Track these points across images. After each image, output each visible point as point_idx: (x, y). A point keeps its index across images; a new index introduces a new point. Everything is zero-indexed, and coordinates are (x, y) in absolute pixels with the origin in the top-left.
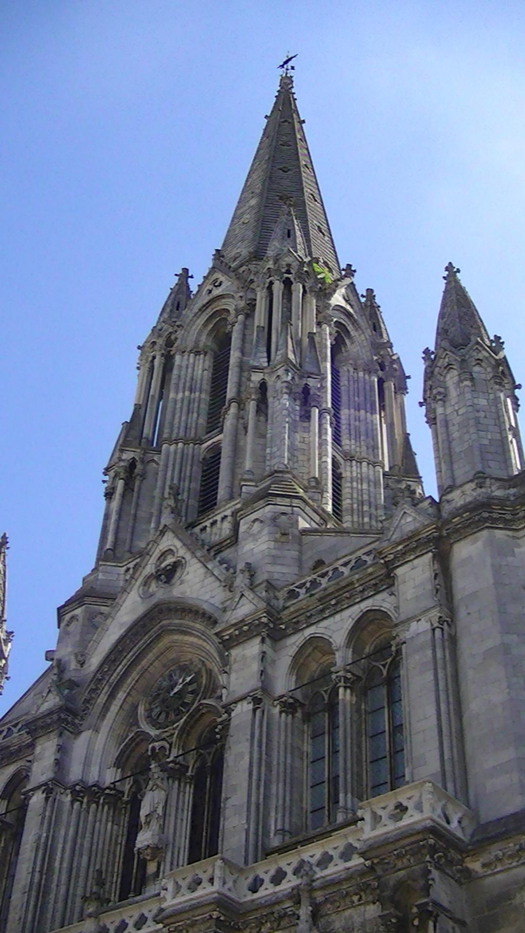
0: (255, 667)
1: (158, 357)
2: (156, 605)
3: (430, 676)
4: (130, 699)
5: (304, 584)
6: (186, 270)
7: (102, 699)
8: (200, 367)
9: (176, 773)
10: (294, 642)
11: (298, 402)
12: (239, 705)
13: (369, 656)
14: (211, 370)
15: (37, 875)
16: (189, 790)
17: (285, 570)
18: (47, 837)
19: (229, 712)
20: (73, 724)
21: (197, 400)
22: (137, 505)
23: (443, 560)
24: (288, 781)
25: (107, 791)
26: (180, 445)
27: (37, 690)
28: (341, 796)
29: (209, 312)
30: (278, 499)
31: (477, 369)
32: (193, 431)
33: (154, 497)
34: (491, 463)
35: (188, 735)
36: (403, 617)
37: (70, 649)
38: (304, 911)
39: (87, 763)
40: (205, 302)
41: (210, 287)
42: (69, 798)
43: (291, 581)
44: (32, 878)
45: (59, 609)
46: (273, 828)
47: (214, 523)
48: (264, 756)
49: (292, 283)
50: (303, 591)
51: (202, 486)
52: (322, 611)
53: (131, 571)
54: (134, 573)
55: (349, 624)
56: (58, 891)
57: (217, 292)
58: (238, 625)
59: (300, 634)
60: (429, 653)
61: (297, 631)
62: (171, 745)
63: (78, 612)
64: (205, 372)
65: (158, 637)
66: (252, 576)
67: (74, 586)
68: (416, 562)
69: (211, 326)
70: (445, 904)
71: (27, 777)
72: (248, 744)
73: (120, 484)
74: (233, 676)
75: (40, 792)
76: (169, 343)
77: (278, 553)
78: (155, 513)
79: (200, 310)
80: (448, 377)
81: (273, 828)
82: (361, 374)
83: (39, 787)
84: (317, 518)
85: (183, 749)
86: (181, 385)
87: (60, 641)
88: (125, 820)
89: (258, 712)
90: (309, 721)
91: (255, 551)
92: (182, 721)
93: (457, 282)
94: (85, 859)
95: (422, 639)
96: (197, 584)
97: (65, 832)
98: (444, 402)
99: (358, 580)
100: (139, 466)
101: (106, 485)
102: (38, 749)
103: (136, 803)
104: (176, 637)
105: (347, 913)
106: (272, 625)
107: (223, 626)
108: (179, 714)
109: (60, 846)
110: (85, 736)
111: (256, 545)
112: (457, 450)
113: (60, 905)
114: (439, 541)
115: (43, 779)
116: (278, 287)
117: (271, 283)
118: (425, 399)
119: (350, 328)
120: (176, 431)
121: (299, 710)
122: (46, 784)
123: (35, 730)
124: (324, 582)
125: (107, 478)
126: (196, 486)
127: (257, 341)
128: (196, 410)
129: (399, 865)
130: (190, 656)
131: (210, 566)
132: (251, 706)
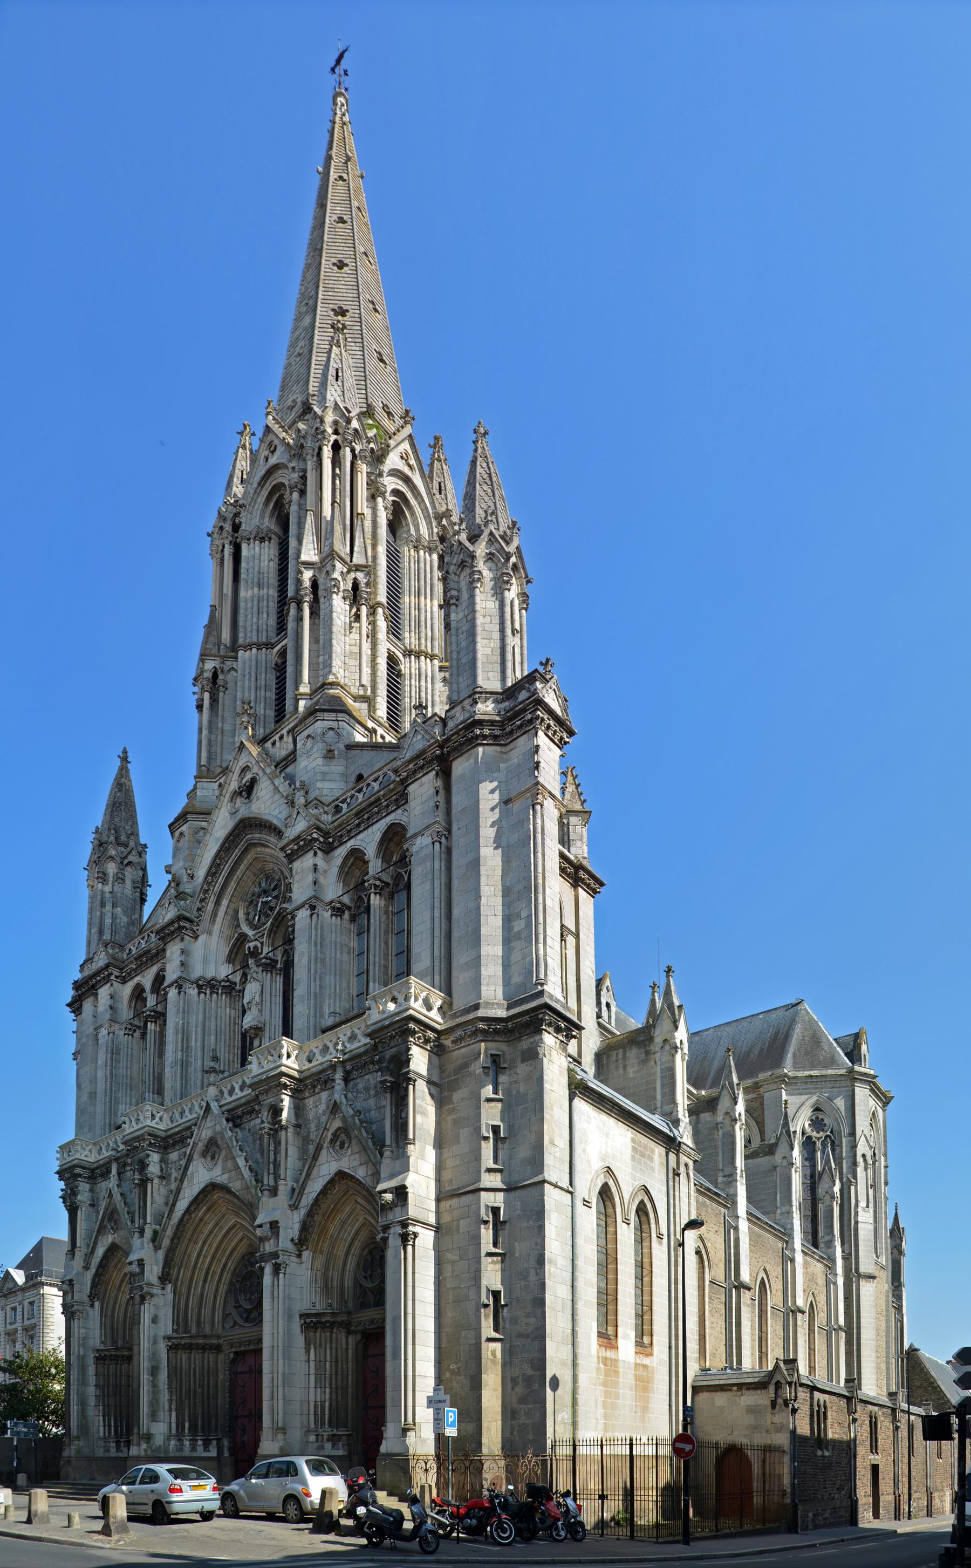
1: (227, 546)
2: (242, 821)
4: (232, 906)
5: (346, 799)
7: (210, 906)
8: (266, 557)
9: (269, 966)
10: (341, 852)
11: (348, 602)
12: (300, 911)
13: (395, 864)
14: (277, 560)
15: (180, 1053)
16: (280, 980)
17: (333, 785)
19: (293, 918)
20: (192, 930)
21: (265, 597)
23: (446, 774)
24: (338, 972)
25: (223, 983)
26: (254, 650)
29: (268, 487)
30: (326, 714)
32: (265, 634)
35: (275, 933)
37: (181, 864)
38: (339, 1076)
39: (205, 961)
40: (263, 472)
42: (196, 991)
45: (170, 826)
49: (340, 448)
50: (344, 806)
51: (277, 694)
52: (359, 825)
58: (297, 839)
59: (344, 846)
60: (429, 864)
61: (342, 844)
62: (262, 943)
63: (184, 828)
64: (272, 563)
65: (246, 850)
66: (307, 793)
68: (423, 779)
69: (272, 504)
71: (164, 977)
73: (207, 696)
75: (173, 988)
79: (259, 484)
82: (422, 552)
83: (302, 906)
85: (273, 945)
86: (250, 581)
89: (315, 916)
90: (355, 921)
94: (213, 1037)
95: (423, 853)
96: (267, 803)
98: (457, 606)
99: (383, 796)
100: (221, 677)
101: (196, 697)
102: (168, 953)
104: (259, 849)
105: (367, 1077)
106: (322, 840)
108: (268, 916)
110: (202, 938)
111: (309, 763)
114: (441, 759)
115: (174, 977)
119: (409, 495)
120: (249, 635)
121: (347, 913)
122: (176, 982)
123: (164, 937)
124: (360, 796)
128: (265, 609)
129: (392, 1044)
130: (271, 865)
131: (276, 784)
132: (309, 912)
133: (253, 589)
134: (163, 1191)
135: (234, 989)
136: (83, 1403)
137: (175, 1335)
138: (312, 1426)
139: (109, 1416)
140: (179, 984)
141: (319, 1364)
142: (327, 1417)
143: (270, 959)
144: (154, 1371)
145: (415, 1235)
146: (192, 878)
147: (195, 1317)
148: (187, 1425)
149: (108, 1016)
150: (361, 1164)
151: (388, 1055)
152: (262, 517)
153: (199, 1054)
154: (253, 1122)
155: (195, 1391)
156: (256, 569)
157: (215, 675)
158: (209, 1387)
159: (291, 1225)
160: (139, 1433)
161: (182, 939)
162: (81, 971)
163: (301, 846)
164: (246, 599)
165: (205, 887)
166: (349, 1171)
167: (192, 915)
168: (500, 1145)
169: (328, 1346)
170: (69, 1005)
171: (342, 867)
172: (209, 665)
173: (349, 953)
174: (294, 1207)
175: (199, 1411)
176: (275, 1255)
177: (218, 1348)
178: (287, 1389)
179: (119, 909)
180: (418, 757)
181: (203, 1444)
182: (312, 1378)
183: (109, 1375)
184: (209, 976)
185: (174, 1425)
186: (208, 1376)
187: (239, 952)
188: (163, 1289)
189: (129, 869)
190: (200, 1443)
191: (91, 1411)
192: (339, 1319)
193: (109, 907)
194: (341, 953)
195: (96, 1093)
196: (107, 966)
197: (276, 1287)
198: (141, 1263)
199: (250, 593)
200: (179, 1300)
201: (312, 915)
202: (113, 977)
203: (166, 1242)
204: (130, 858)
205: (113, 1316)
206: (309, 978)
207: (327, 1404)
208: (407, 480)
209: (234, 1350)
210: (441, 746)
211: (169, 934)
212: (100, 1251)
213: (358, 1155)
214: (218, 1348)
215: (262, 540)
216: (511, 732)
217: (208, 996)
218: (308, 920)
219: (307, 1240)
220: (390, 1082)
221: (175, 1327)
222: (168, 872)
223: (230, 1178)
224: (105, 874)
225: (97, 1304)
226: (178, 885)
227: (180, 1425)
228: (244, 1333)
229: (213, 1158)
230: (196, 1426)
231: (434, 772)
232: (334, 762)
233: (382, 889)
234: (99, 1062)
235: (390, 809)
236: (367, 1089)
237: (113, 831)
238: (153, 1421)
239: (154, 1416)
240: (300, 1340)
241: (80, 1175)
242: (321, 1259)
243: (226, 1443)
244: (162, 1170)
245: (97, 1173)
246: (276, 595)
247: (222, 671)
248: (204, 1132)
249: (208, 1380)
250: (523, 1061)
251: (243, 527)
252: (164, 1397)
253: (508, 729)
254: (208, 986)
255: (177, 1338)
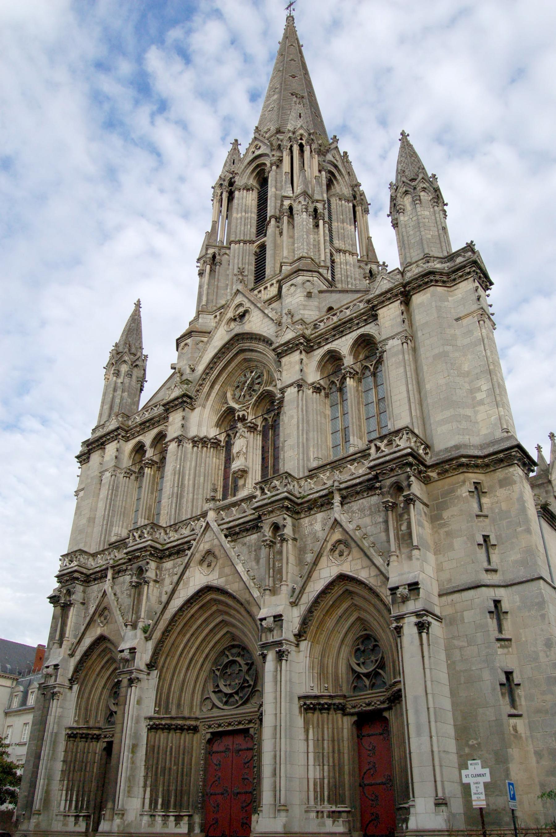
0: (298, 367)
2: (237, 335)
3: (402, 370)
6: (236, 141)
10: (319, 353)
12: (289, 389)
14: (256, 200)
15: (176, 489)
16: (260, 438)
17: (311, 313)
18: (180, 468)
22: (218, 279)
23: (407, 302)
24: (319, 430)
25: (212, 441)
26: (242, 244)
27: (167, 386)
28: (351, 438)
29: (254, 165)
31: (422, 194)
33: (228, 275)
34: (433, 249)
36: (384, 337)
37: (185, 362)
38: (337, 499)
39: (200, 425)
40: (251, 158)
41: (253, 150)
42: (191, 445)
43: (315, 319)
44: (173, 490)
45: (177, 340)
46: (312, 457)
47: (266, 288)
48: (305, 417)
50: (322, 324)
52: (334, 336)
53: (218, 317)
54: (221, 318)
55: (351, 342)
56: (188, 497)
57: (257, 153)
59: (322, 349)
60: (401, 357)
63: (189, 341)
66: (292, 316)
67: (184, 328)
68: (390, 306)
70: (419, 495)
72: (295, 411)
74: (284, 373)
75: (174, 442)
76: (231, 184)
77: (306, 303)
78: (230, 284)
80: (405, 199)
81: (312, 457)
82: (343, 202)
83: (173, 440)
84: (327, 283)
86: (240, 209)
87: (179, 357)
88: (223, 456)
89: (301, 392)
91: (293, 303)
92: (254, 400)
93: (408, 142)
94: (202, 478)
96: (256, 323)
97: (190, 465)
100: (218, 257)
102: (171, 419)
103: (229, 445)
107: (277, 345)
109: (187, 472)
110: (198, 410)
112: (413, 241)
113: (190, 505)
115: (175, 435)
116: (296, 149)
117: (291, 146)
118: (391, 213)
121: (323, 391)
122: (177, 438)
125: (199, 264)
126: (253, 268)
127: (286, 181)
132: (296, 389)
133: (241, 213)
134: (156, 592)
135: (219, 445)
136: (49, 778)
137: (156, 715)
138: (312, 802)
139: (72, 790)
140: (179, 440)
141: (319, 742)
142: (326, 793)
143: (253, 423)
144: (134, 749)
145: (429, 623)
146: (193, 371)
147: (175, 701)
148: (160, 801)
149: (113, 463)
150: (363, 568)
151: (388, 482)
152: (249, 178)
153: (191, 489)
154: (248, 538)
155: (170, 769)
156: (244, 203)
157: (214, 257)
158: (183, 765)
159: (293, 619)
160: (113, 809)
161: (184, 409)
162: (92, 433)
163: (283, 351)
164: (237, 219)
165: (204, 376)
166: (351, 574)
167: (192, 394)
168: (491, 551)
169: (326, 726)
170: (77, 457)
171: (320, 362)
172: (211, 251)
173: (325, 418)
174: (294, 604)
175: (173, 787)
176: (279, 643)
177: (195, 729)
178: (288, 766)
179: (126, 393)
180: (386, 292)
181: (175, 820)
182: (311, 756)
183: (77, 752)
184: (202, 435)
185: (147, 801)
186: (184, 754)
187: (229, 419)
188: (149, 674)
189: (136, 369)
190: (172, 819)
191: (56, 785)
192: (336, 701)
193: (119, 392)
194: (321, 417)
195: (95, 518)
196: (118, 429)
197: (279, 672)
198: (133, 650)
199: (239, 215)
200: (163, 685)
201: (299, 391)
202: (120, 437)
203: (157, 635)
204: (137, 363)
205: (88, 698)
206: (298, 432)
207: (326, 781)
208: (336, 167)
209: (211, 730)
210: (404, 286)
211: (173, 407)
212: (87, 641)
213: (359, 561)
214: (195, 729)
215: (248, 190)
216: (454, 280)
217: (200, 449)
218: (296, 394)
219: (305, 632)
220: (392, 502)
221: (77, 719)
222: (172, 368)
223: (227, 581)
224: (119, 371)
225: (76, 687)
226: (182, 375)
227: (153, 802)
228: (229, 714)
229: (209, 566)
230: (169, 801)
231: (399, 301)
232: (312, 300)
233: (354, 375)
234: (101, 496)
235: (360, 325)
236: (362, 510)
237: (128, 346)
238: (129, 796)
239: (129, 792)
240: (300, 721)
241: (77, 579)
242: (318, 649)
243: (197, 819)
244: (157, 575)
245: (90, 578)
246: (256, 217)
247: (219, 255)
248: (202, 545)
249: (183, 759)
250: (501, 486)
251: (236, 183)
252: (141, 772)
253: (453, 277)
254: (201, 442)
255: (159, 718)
